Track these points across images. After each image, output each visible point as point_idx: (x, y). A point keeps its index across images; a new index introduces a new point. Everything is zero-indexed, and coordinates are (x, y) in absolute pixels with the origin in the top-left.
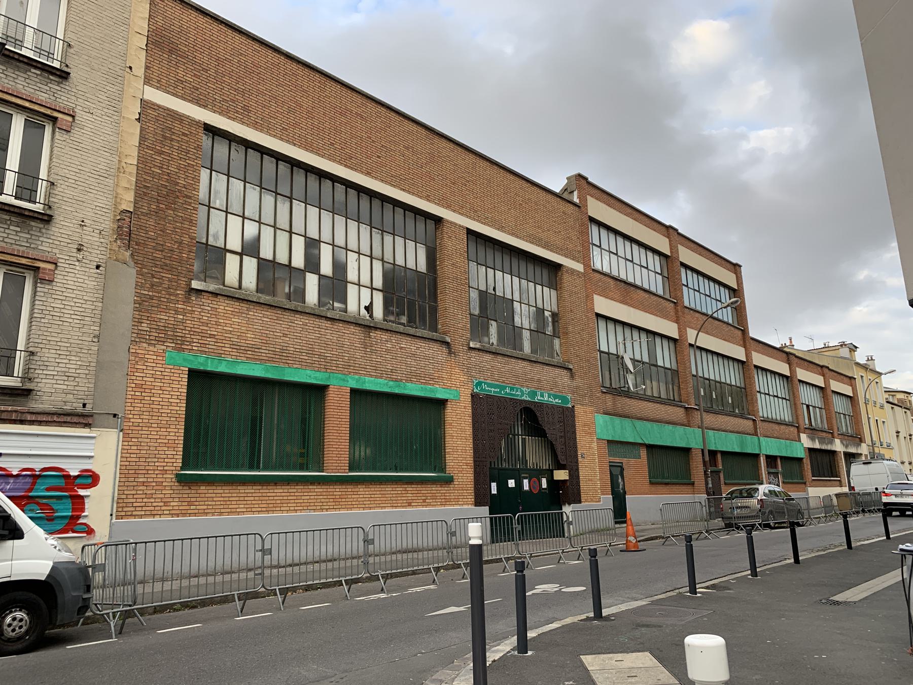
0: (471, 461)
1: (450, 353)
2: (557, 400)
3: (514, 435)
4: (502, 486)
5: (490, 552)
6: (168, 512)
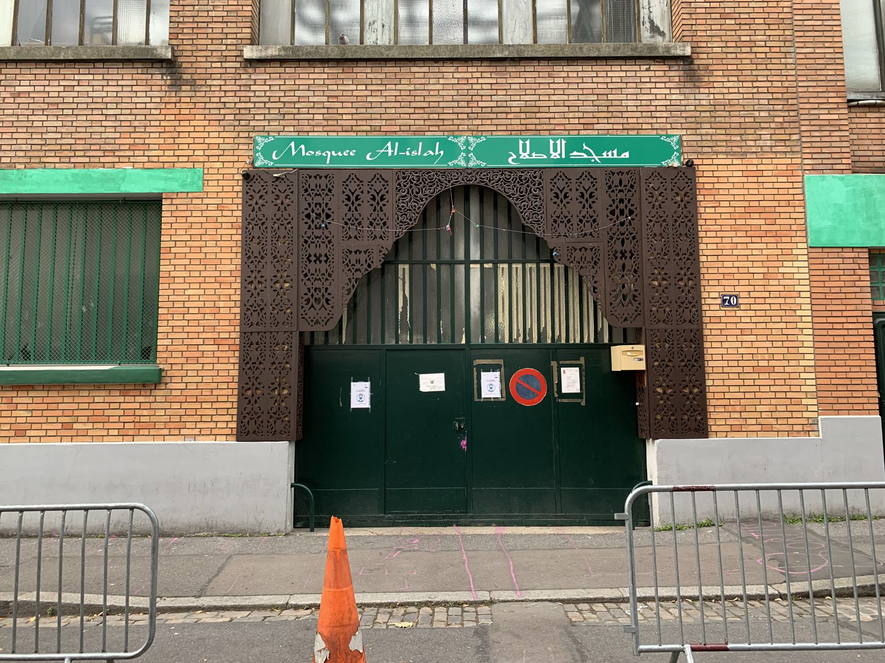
0: (231, 332)
1: (177, 84)
2: (612, 154)
3: (452, 263)
4: (394, 387)
5: (50, 571)
6: (116, 432)
